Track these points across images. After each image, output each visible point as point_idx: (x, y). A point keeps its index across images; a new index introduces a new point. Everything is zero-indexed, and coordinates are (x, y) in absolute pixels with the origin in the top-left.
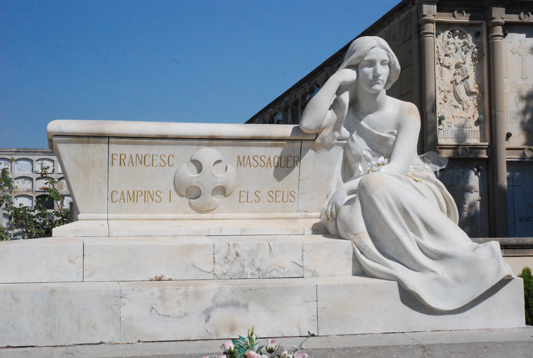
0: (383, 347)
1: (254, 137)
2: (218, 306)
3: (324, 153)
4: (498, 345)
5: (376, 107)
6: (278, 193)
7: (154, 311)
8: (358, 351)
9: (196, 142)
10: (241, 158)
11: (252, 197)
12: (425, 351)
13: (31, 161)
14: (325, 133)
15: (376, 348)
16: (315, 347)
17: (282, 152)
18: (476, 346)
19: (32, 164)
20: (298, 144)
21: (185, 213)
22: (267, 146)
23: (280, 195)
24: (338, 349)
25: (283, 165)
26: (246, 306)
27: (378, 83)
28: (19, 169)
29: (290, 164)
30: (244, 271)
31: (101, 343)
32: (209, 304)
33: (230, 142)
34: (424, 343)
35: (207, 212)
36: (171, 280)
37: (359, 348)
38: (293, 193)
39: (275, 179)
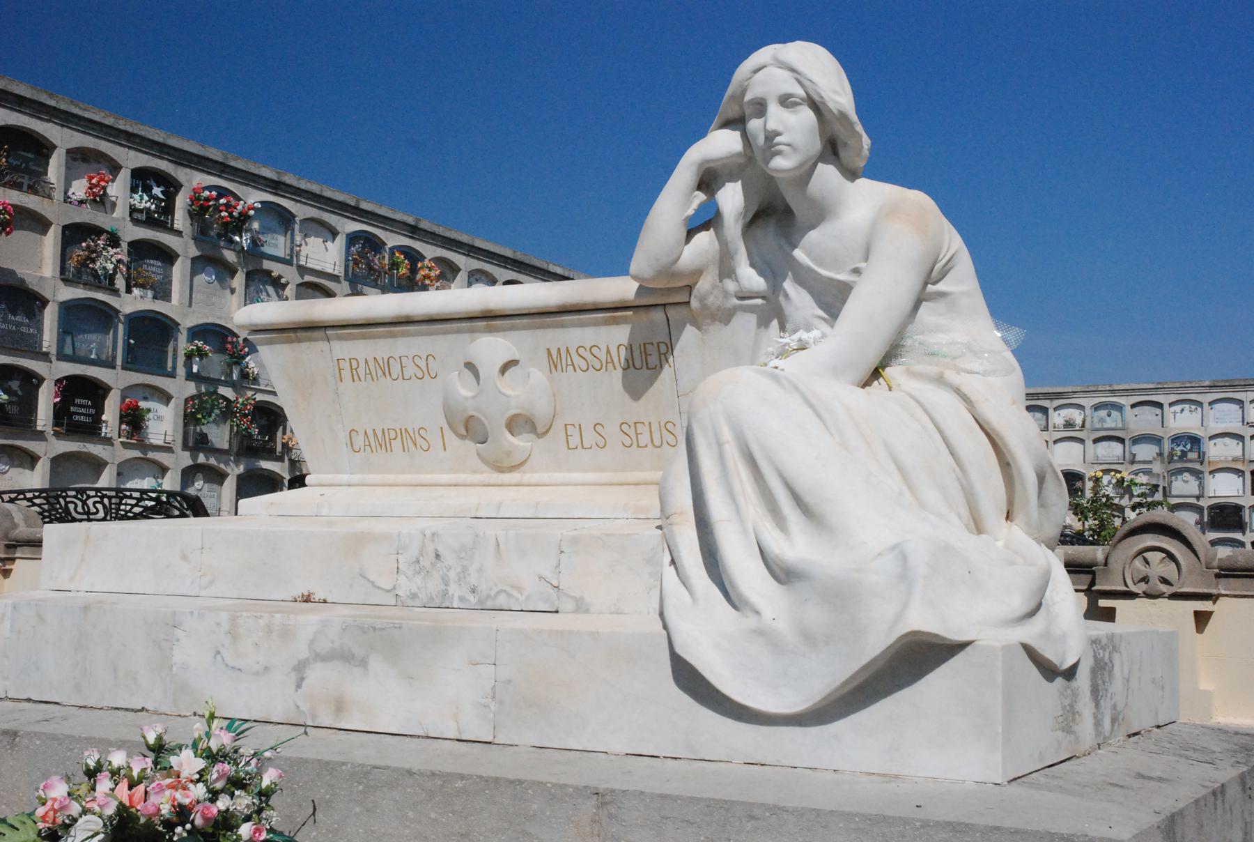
0: (512, 782)
1: (564, 306)
2: (326, 658)
3: (718, 332)
4: (785, 816)
5: (821, 213)
6: (640, 428)
7: (219, 657)
8: (459, 784)
9: (465, 325)
10: (554, 353)
11: (590, 437)
12: (604, 804)
13: (1240, 402)
14: (704, 285)
15: (497, 780)
16: (378, 763)
17: (631, 334)
18: (727, 810)
19: (1242, 408)
20: (658, 315)
21: (474, 472)
22: (596, 323)
23: (643, 429)
24: (422, 774)
25: (638, 364)
26: (364, 663)
27: (779, 153)
28: (1217, 420)
29: (653, 360)
30: (446, 592)
31: (143, 709)
32: (304, 653)
33: (525, 321)
34: (603, 786)
35: (513, 468)
36: (325, 602)
37: (462, 777)
38: (670, 426)
39: (627, 397)
